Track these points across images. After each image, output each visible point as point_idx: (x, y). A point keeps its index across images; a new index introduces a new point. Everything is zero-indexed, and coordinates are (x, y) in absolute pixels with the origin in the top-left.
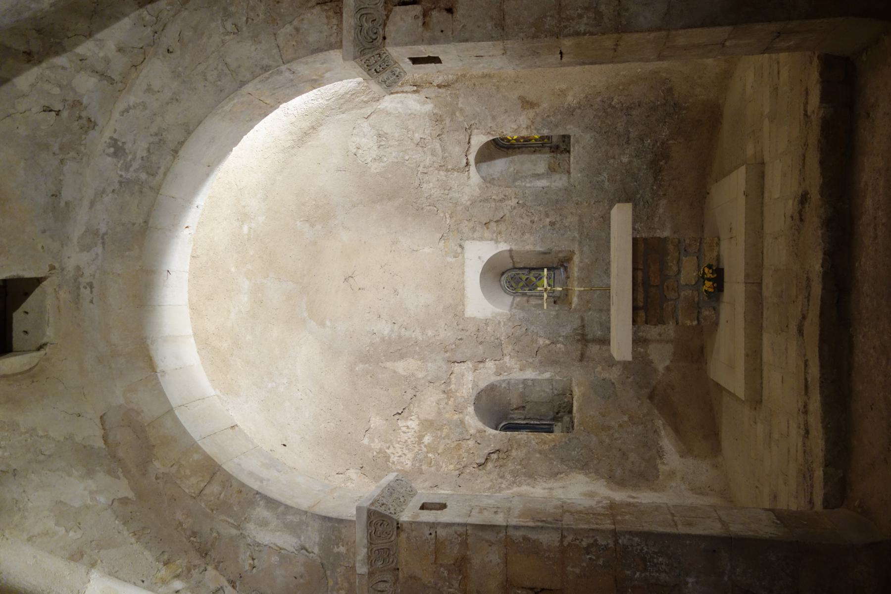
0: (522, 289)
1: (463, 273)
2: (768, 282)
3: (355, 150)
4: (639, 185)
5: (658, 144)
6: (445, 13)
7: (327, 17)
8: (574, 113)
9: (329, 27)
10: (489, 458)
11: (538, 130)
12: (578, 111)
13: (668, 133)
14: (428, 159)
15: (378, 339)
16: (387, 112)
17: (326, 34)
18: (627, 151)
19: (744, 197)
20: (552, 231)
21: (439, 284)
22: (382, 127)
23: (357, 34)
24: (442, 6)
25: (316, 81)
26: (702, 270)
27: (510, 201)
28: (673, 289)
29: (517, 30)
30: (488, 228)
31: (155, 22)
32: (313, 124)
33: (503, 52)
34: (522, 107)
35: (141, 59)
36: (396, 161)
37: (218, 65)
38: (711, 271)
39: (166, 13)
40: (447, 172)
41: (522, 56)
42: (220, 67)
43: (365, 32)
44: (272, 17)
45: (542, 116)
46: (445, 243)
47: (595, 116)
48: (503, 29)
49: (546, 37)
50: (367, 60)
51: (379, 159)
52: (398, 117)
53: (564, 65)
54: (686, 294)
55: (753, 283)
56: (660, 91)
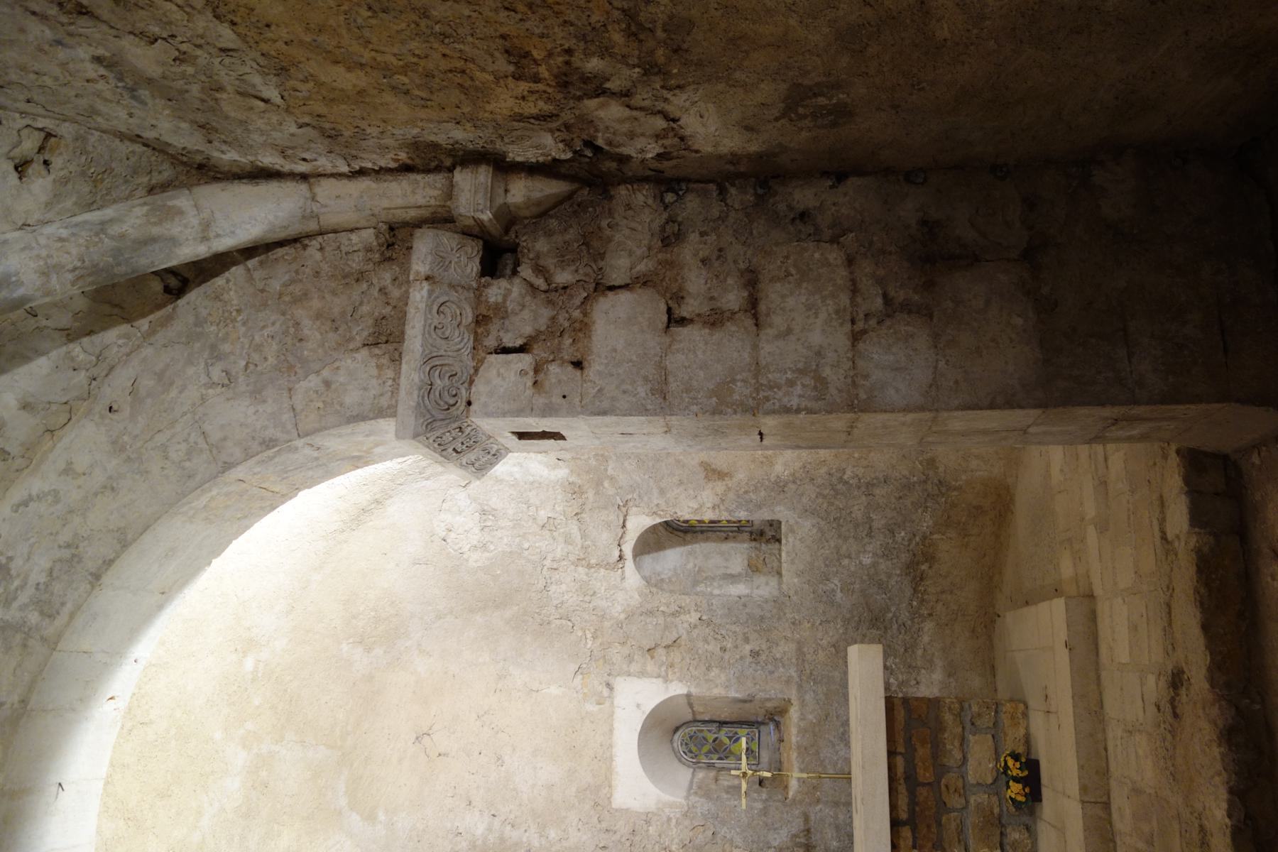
0: (707, 756)
1: (611, 731)
2: (1123, 820)
3: (444, 533)
4: (889, 599)
5: (917, 539)
6: (570, 368)
7: (378, 366)
8: (786, 489)
9: (380, 381)
10: (753, 312)
11: (730, 512)
12: (793, 487)
13: (931, 523)
15: (464, 844)
16: (496, 478)
17: (373, 392)
18: (869, 548)
19: (1067, 651)
20: (754, 665)
21: (570, 749)
23: (423, 397)
24: (566, 357)
25: (359, 458)
26: (1002, 759)
27: (688, 616)
28: (956, 791)
29: (687, 400)
30: (652, 657)
31: (94, 363)
32: (376, 497)
33: (666, 429)
34: (706, 477)
35: (63, 419)
36: (509, 550)
37: (189, 434)
38: (1018, 765)
39: (115, 349)
40: (589, 569)
41: (696, 436)
43: (437, 394)
44: (288, 362)
45: (737, 491)
46: (583, 679)
47: (819, 495)
48: (665, 398)
49: (735, 412)
50: (438, 437)
52: (513, 485)
54: (980, 801)
55: (1096, 803)
56: (917, 462)
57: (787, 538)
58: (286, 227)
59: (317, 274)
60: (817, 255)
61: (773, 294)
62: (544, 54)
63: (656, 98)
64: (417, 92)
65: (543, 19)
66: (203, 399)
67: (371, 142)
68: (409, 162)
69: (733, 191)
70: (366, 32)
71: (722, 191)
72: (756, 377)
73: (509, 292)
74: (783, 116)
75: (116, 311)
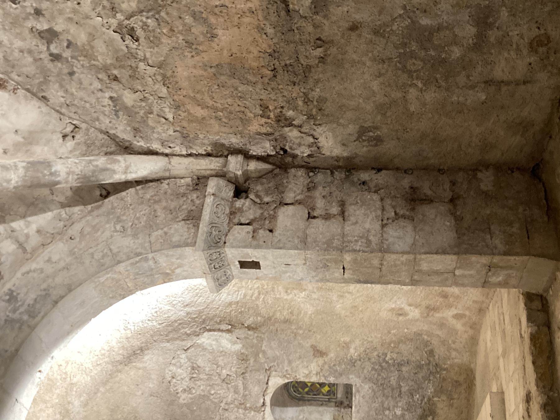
5: (426, 399)
6: (268, 232)
7: (188, 228)
8: (355, 364)
11: (325, 377)
12: (358, 362)
13: (432, 390)
14: (230, 396)
16: (203, 347)
17: (185, 237)
22: (196, 361)
33: (304, 262)
35: (49, 241)
36: (203, 394)
39: (76, 215)
42: (105, 251)
47: (373, 369)
49: (334, 250)
51: (188, 390)
52: (211, 352)
53: (346, 281)
57: (355, 396)
58: (157, 173)
59: (166, 193)
60: (369, 197)
61: (350, 209)
62: (274, 107)
63: (311, 128)
64: (224, 120)
65: (276, 94)
66: (112, 236)
67: (199, 141)
68: (210, 152)
69: (336, 173)
70: (214, 95)
71: (332, 173)
72: (343, 238)
73: (244, 204)
74: (357, 139)
75: (80, 200)
